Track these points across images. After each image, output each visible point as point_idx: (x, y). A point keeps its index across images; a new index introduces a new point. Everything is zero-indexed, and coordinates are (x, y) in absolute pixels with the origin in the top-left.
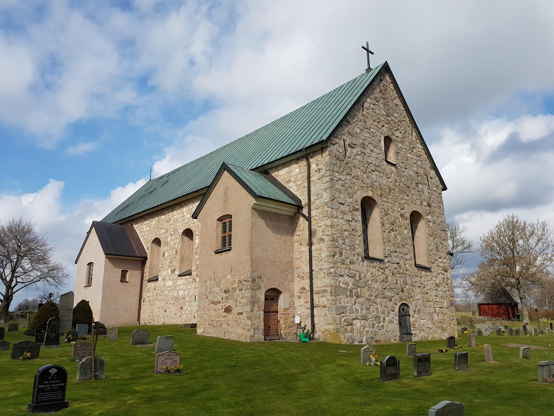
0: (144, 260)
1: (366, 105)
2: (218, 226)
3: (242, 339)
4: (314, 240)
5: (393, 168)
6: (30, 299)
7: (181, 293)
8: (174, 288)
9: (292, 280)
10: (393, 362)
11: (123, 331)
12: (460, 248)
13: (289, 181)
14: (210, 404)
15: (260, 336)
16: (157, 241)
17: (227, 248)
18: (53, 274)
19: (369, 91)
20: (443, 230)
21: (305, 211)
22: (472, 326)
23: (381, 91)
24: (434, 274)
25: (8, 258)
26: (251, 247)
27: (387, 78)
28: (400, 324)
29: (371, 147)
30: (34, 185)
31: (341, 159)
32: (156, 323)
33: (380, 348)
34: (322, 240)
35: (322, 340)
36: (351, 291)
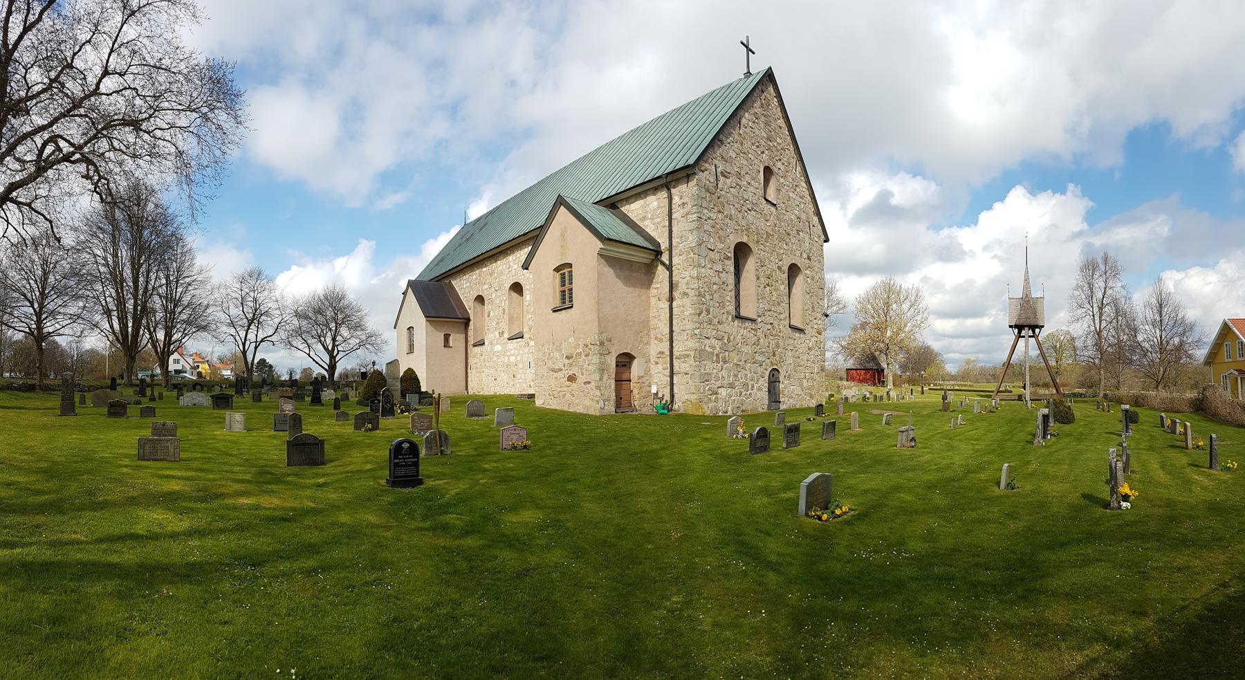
1: (744, 121)
2: (554, 277)
3: (592, 412)
4: (676, 294)
5: (773, 209)
6: (349, 367)
7: (513, 358)
8: (504, 353)
9: (648, 343)
10: (763, 434)
11: (456, 401)
12: (835, 308)
13: (644, 218)
14: (570, 486)
15: (610, 408)
17: (568, 304)
18: (370, 340)
19: (748, 104)
20: (820, 289)
21: (665, 258)
22: (839, 392)
23: (762, 106)
24: (808, 336)
25: (327, 325)
26: (598, 303)
27: (771, 89)
28: (769, 391)
29: (748, 178)
30: (347, 249)
31: (711, 191)
32: (486, 393)
33: (749, 418)
34: (686, 294)
36: (717, 355)
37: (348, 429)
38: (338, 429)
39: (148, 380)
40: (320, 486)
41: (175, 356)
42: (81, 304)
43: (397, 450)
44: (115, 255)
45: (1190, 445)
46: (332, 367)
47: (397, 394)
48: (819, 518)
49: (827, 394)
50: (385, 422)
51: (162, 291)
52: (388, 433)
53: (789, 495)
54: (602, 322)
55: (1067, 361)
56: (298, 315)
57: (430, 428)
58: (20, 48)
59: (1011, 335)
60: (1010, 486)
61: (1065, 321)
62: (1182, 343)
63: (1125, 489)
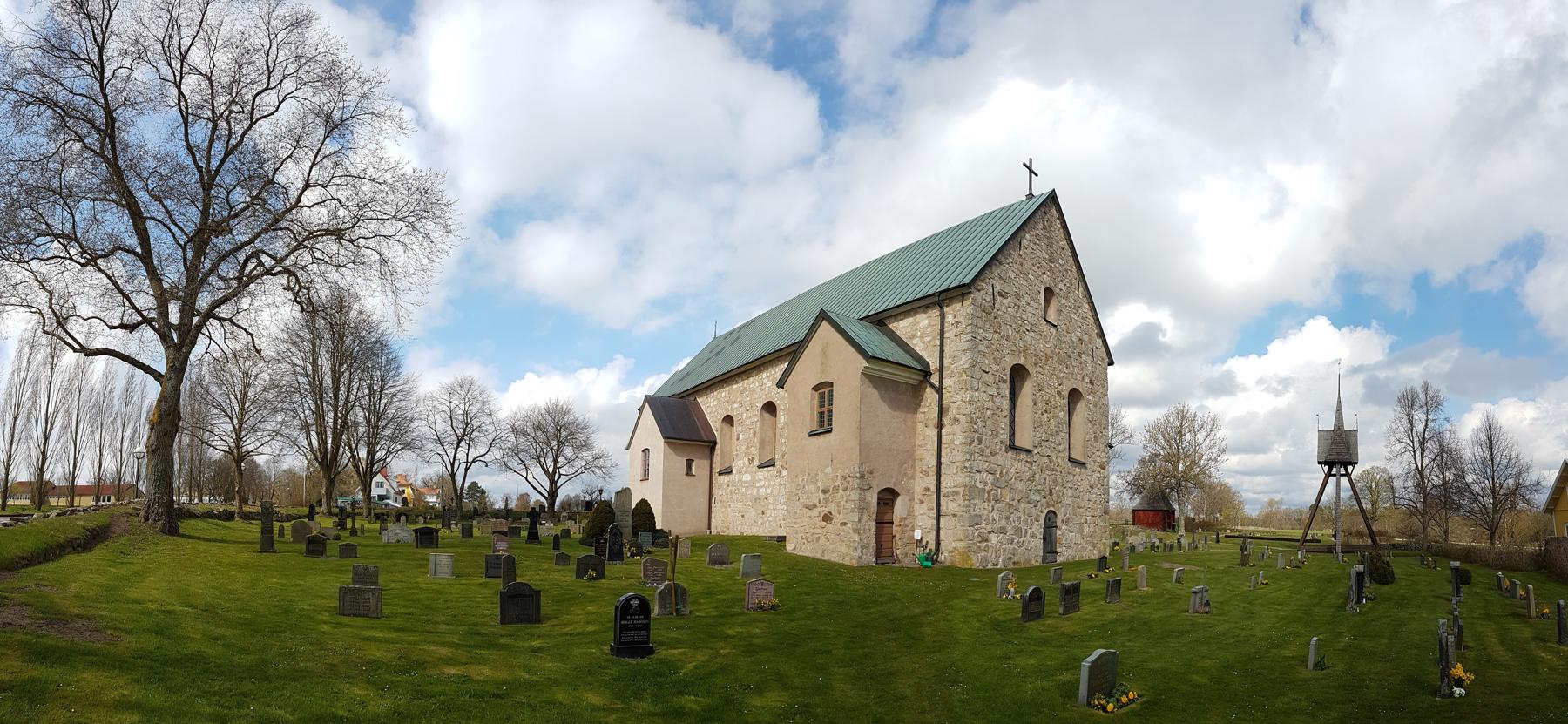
0: (713, 444)
1: (1024, 242)
3: (847, 562)
4: (946, 420)
9: (913, 477)
10: (1037, 596)
11: (699, 543)
12: (1119, 438)
13: (913, 336)
14: (820, 660)
15: (870, 558)
16: (729, 420)
18: (597, 463)
19: (1030, 225)
20: (1102, 417)
21: (935, 379)
22: (1124, 540)
24: (1089, 472)
25: (548, 444)
28: (1045, 539)
30: (600, 363)
31: (988, 311)
33: (1021, 572)
35: (948, 563)
37: (567, 576)
38: (558, 576)
39: (349, 508)
40: (535, 650)
41: (379, 478)
42: (280, 419)
43: (624, 609)
44: (315, 363)
45: (1533, 614)
46: (553, 494)
47: (627, 531)
48: (1104, 709)
49: (1110, 542)
50: (612, 568)
51: (365, 402)
52: (615, 584)
53: (1066, 677)
54: (865, 451)
55: (1384, 506)
56: (515, 430)
57: (664, 578)
58: (222, 172)
59: (1321, 471)
60: (1319, 666)
61: (1382, 454)
62: (1518, 486)
63: (1459, 671)
